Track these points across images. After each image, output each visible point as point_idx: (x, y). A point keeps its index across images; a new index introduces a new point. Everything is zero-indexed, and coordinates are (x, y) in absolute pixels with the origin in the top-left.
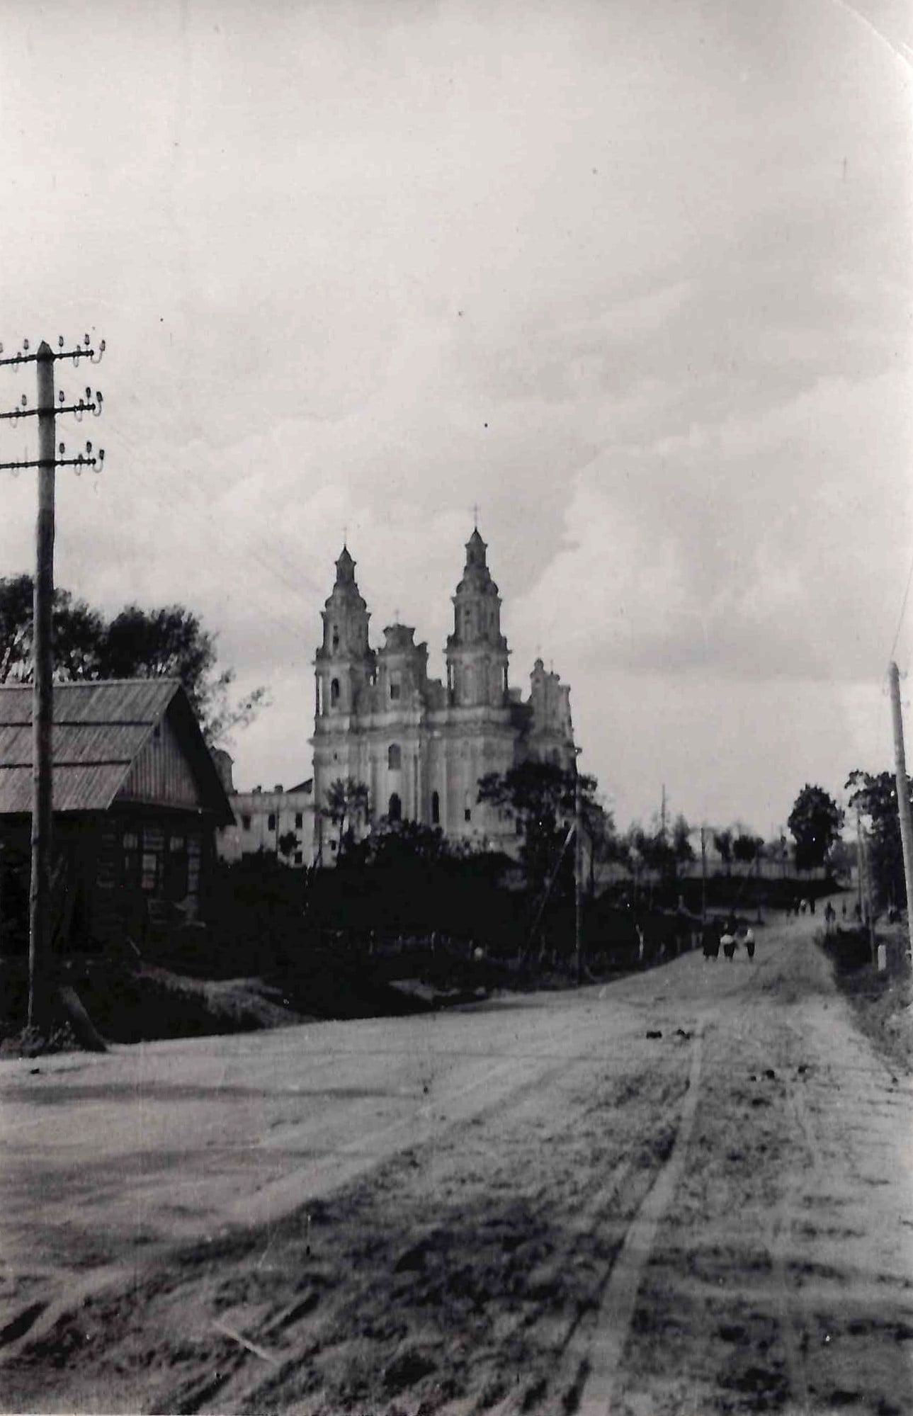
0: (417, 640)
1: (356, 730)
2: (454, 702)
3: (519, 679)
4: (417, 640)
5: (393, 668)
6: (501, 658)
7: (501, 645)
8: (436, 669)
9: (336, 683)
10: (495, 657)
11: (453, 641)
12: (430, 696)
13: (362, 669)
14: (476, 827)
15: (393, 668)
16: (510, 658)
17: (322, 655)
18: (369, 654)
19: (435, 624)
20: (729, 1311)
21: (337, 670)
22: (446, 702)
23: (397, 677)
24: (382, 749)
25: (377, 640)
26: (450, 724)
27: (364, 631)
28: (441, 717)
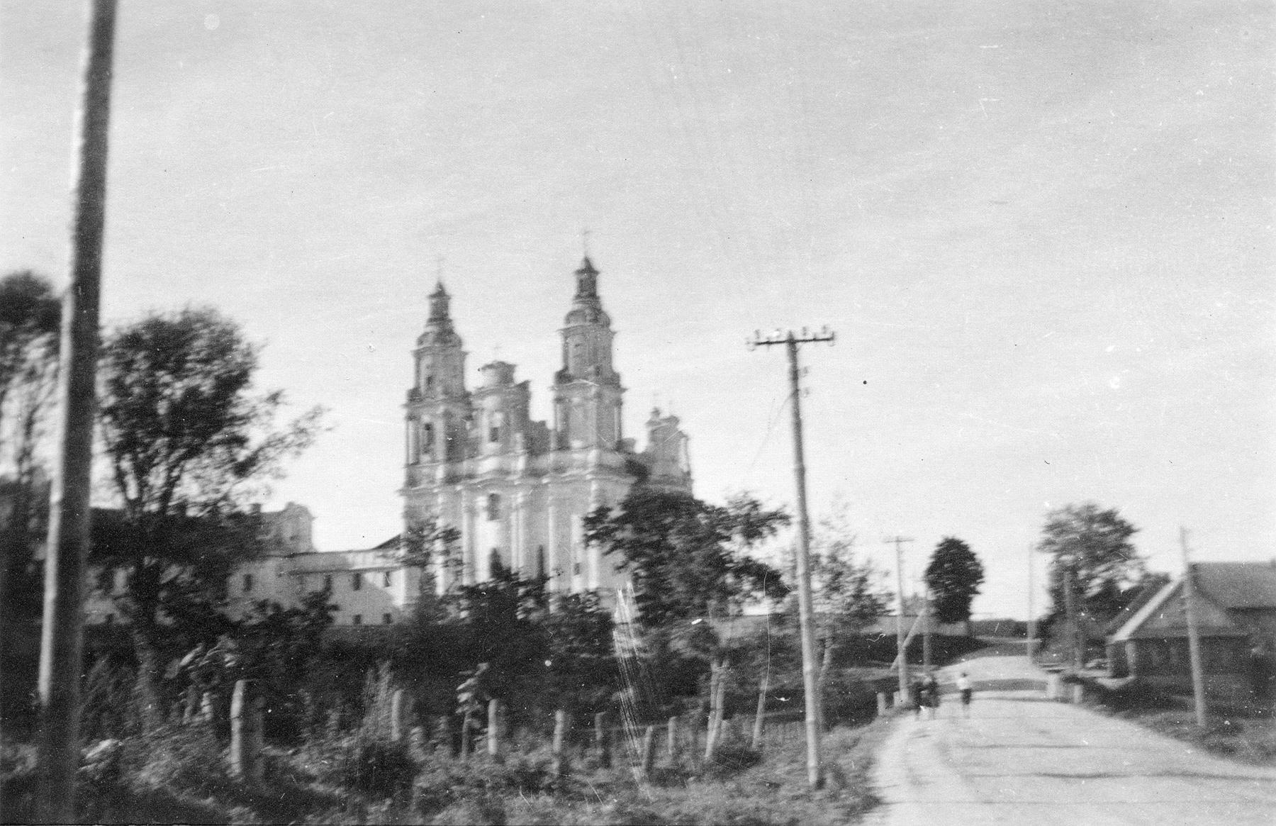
0: (519, 377)
1: (452, 479)
2: (563, 446)
3: (639, 438)
4: (519, 377)
5: (490, 414)
6: (613, 395)
7: (613, 381)
8: (542, 409)
9: (428, 427)
10: (609, 394)
11: (563, 377)
12: (536, 440)
13: (459, 412)
14: (595, 576)
15: (490, 414)
16: (626, 397)
17: (414, 396)
18: (465, 397)
19: (539, 363)
20: (728, 615)
21: (434, 415)
22: (553, 445)
23: (498, 419)
24: (482, 501)
25: (474, 380)
26: (559, 469)
27: (459, 372)
28: (550, 459)
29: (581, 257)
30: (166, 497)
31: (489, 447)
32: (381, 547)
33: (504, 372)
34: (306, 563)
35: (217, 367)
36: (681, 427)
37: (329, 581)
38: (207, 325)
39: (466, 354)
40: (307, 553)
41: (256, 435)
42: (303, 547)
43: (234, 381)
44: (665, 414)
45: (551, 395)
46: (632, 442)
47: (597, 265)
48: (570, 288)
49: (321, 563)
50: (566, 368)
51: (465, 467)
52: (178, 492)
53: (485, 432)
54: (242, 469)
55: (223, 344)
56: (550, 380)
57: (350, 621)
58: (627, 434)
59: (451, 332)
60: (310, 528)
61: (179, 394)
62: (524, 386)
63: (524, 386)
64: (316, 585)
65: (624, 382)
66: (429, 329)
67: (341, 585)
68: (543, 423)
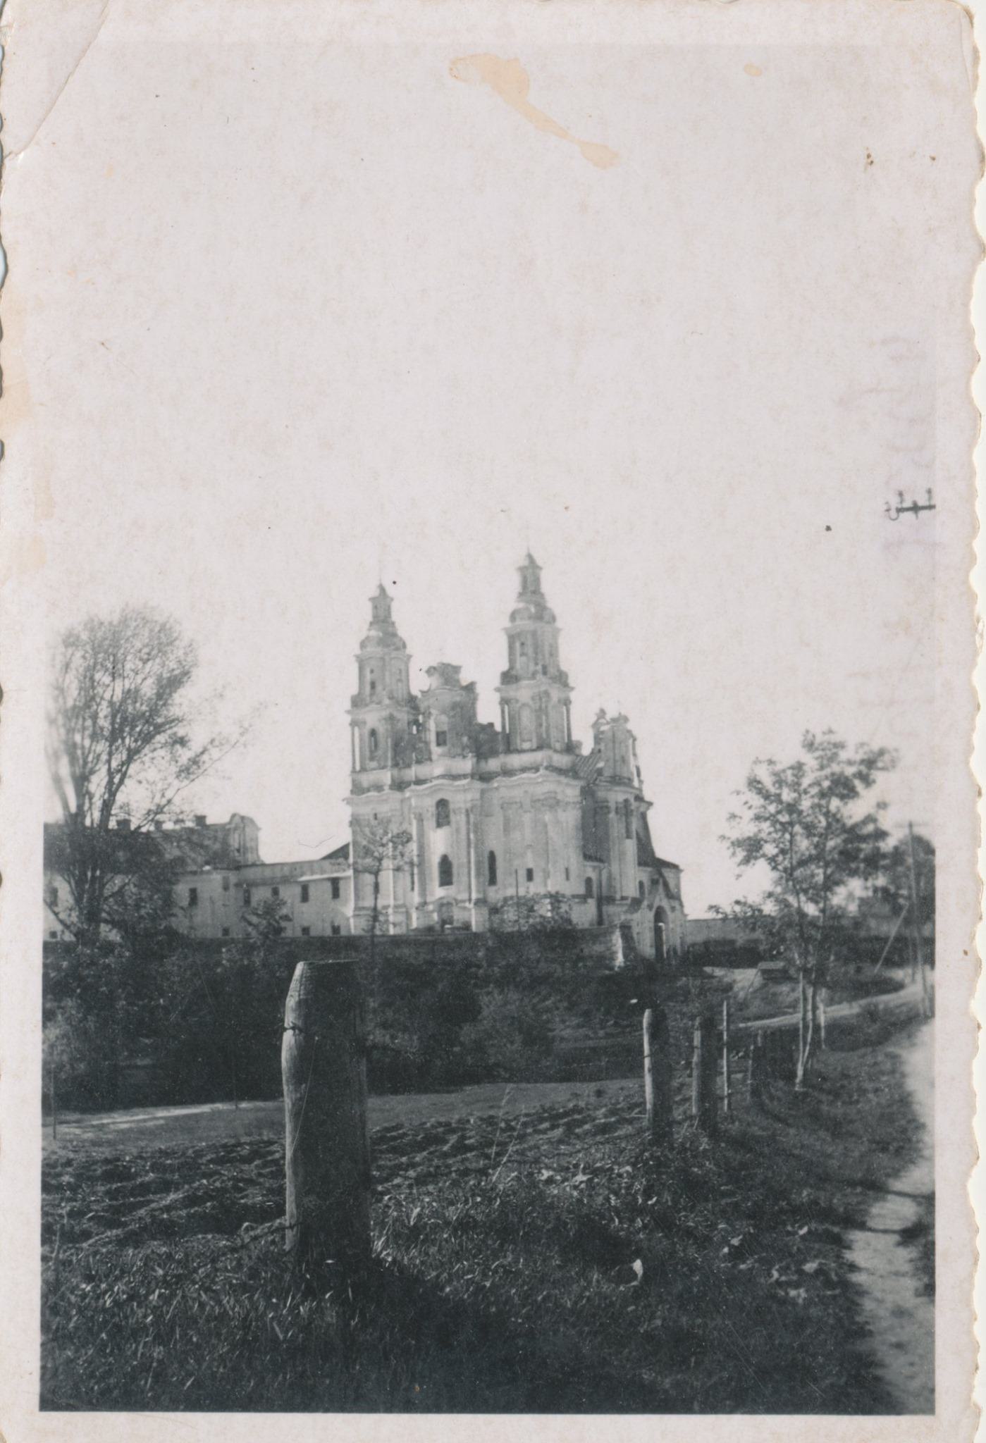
11: (508, 678)
17: (357, 702)
19: (483, 668)
22: (501, 748)
27: (404, 677)
29: (524, 553)
30: (107, 806)
31: (436, 750)
32: (330, 857)
33: (447, 673)
34: (250, 874)
35: (154, 667)
36: (629, 726)
37: (275, 892)
38: (146, 621)
39: (410, 657)
40: (254, 865)
41: (198, 736)
42: (250, 858)
43: (170, 684)
44: (611, 713)
45: (496, 697)
46: (579, 745)
47: (539, 562)
48: (513, 583)
49: (268, 873)
50: (512, 668)
51: (412, 772)
52: (120, 798)
53: (432, 737)
54: (189, 770)
55: (162, 640)
56: (497, 682)
57: (299, 933)
58: (576, 736)
59: (395, 635)
60: (256, 839)
61: (118, 695)
62: (470, 688)
63: (470, 688)
64: (261, 895)
65: (571, 682)
66: (373, 633)
67: (290, 894)
68: (491, 725)
